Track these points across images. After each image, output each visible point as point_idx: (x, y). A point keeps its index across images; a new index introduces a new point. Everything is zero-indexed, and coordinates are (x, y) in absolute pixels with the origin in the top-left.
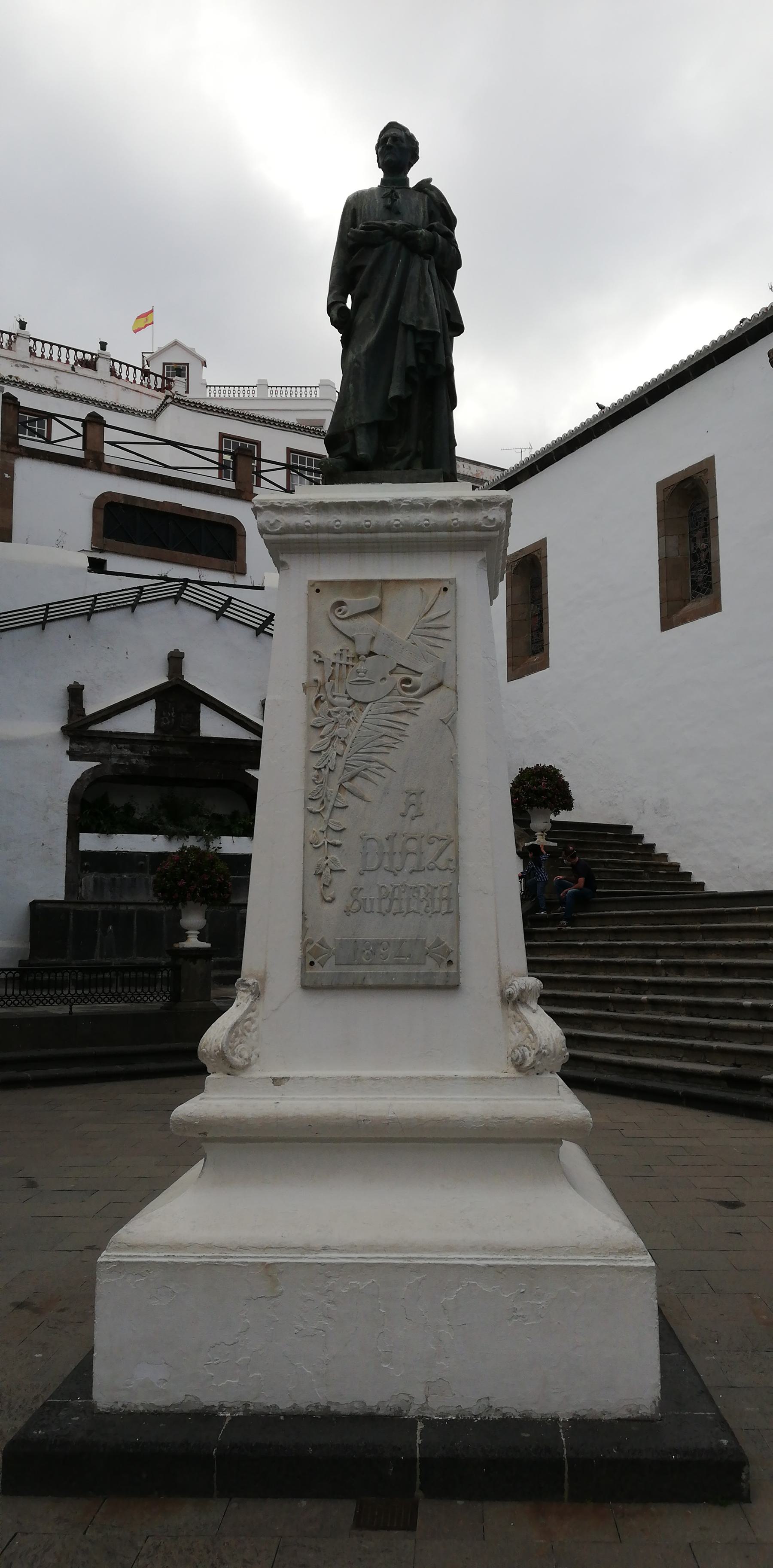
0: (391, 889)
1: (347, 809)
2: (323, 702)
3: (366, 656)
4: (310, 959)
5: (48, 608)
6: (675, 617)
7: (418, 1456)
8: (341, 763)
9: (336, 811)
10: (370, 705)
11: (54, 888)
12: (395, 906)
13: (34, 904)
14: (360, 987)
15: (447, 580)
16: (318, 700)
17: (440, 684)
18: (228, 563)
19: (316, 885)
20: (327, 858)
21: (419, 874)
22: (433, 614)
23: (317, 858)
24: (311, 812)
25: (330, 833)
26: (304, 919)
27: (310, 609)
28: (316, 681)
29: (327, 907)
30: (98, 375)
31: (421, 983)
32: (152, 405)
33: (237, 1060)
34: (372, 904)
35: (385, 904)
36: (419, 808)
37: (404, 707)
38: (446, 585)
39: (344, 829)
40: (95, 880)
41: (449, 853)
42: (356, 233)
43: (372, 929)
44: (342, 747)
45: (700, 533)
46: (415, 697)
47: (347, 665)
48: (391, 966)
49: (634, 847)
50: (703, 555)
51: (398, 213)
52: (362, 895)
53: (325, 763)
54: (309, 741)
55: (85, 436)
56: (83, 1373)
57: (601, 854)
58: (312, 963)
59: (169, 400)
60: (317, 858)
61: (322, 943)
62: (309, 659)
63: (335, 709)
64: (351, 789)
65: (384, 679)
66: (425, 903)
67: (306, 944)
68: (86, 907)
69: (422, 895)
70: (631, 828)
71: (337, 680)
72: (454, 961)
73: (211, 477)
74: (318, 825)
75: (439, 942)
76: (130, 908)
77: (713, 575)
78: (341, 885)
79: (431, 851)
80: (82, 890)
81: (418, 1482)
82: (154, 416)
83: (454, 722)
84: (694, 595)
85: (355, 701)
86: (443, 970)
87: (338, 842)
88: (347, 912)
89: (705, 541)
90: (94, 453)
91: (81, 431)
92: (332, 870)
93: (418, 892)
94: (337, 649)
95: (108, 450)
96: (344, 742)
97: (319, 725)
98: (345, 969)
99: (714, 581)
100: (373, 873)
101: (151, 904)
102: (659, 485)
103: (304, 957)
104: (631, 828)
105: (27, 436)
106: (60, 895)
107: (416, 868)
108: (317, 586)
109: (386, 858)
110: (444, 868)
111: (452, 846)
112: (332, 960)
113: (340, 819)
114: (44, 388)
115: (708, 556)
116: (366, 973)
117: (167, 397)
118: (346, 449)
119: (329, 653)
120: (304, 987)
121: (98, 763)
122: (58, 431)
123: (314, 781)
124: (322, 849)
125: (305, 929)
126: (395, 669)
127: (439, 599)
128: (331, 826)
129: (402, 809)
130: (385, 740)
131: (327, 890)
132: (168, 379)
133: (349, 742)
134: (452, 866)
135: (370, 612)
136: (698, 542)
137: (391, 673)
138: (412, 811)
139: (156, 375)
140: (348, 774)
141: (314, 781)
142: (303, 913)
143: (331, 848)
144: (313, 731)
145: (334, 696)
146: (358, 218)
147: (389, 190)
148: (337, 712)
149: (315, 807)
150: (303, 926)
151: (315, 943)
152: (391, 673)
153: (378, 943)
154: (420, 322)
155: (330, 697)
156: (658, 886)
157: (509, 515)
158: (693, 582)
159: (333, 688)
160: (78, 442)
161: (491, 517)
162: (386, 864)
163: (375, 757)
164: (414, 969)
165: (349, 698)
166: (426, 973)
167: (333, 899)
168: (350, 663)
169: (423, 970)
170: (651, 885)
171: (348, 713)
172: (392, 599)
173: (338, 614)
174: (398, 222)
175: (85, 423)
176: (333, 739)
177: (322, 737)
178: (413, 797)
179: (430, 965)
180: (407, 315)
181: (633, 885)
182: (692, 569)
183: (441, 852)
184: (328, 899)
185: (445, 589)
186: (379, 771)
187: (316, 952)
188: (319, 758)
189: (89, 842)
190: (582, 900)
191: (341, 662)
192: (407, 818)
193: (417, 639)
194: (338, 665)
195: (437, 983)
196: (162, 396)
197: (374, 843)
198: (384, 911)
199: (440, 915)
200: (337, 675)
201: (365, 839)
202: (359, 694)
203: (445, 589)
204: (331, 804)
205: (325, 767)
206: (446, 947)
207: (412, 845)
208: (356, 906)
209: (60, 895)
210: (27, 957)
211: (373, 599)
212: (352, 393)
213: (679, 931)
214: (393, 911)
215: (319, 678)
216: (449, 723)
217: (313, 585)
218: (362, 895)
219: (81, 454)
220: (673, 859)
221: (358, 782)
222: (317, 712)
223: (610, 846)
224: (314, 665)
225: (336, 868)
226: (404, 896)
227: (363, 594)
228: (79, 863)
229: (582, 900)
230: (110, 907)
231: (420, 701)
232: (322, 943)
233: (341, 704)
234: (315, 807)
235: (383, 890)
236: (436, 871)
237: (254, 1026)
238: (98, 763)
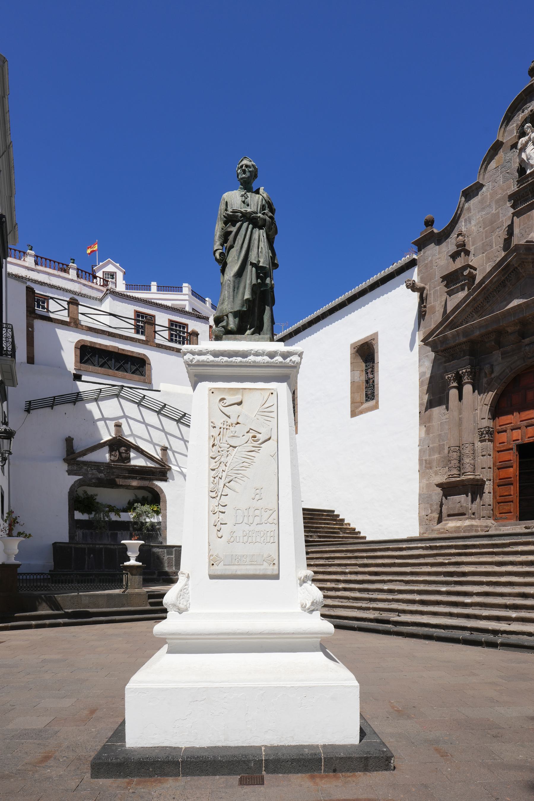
5: (55, 399)
6: (357, 411)
7: (264, 753)
8: (224, 474)
11: (64, 537)
13: (55, 544)
16: (213, 445)
18: (142, 377)
22: (266, 405)
30: (70, 277)
32: (100, 295)
33: (181, 606)
35: (246, 538)
37: (254, 449)
38: (272, 391)
40: (83, 533)
42: (228, 214)
45: (370, 370)
49: (335, 520)
50: (371, 381)
51: (248, 205)
52: (235, 535)
54: (210, 464)
55: (68, 310)
56: (119, 733)
57: (321, 523)
58: (213, 565)
59: (108, 292)
62: (209, 426)
63: (222, 449)
65: (244, 435)
66: (263, 538)
67: (210, 556)
68: (80, 546)
69: (262, 535)
70: (333, 511)
73: (131, 333)
76: (101, 546)
77: (375, 391)
79: (266, 515)
80: (77, 538)
81: (264, 769)
82: (101, 300)
84: (367, 400)
85: (231, 446)
87: (223, 511)
88: (229, 542)
89: (372, 374)
90: (74, 318)
91: (67, 307)
94: (222, 421)
95: (81, 317)
97: (214, 457)
99: (375, 394)
101: (111, 545)
102: (352, 345)
104: (333, 511)
105: (41, 309)
106: (67, 540)
109: (246, 518)
114: (44, 283)
115: (373, 382)
117: (107, 290)
118: (224, 323)
119: (218, 424)
121: (81, 477)
122: (53, 306)
125: (210, 550)
129: (253, 497)
132: (106, 280)
136: (369, 374)
137: (247, 432)
138: (257, 497)
139: (100, 278)
140: (228, 480)
146: (229, 206)
147: (244, 193)
148: (222, 451)
149: (213, 495)
152: (247, 432)
154: (259, 261)
156: (346, 538)
157: (301, 358)
158: (366, 394)
160: (66, 313)
161: (293, 360)
162: (246, 520)
163: (240, 472)
164: (258, 567)
165: (228, 444)
168: (228, 427)
169: (262, 567)
170: (343, 537)
171: (228, 451)
173: (223, 404)
174: (249, 210)
175: (69, 303)
180: (253, 258)
181: (335, 537)
182: (366, 388)
184: (220, 536)
185: (272, 393)
186: (242, 478)
189: (78, 515)
193: (259, 417)
194: (222, 428)
196: (104, 289)
202: (233, 442)
203: (272, 393)
206: (272, 557)
208: (232, 539)
209: (67, 540)
210: (53, 569)
211: (237, 398)
212: (226, 296)
213: (356, 558)
219: (68, 319)
220: (352, 526)
223: (325, 519)
226: (254, 535)
227: (234, 395)
228: (74, 524)
230: (91, 546)
231: (261, 446)
237: (187, 592)
238: (81, 477)
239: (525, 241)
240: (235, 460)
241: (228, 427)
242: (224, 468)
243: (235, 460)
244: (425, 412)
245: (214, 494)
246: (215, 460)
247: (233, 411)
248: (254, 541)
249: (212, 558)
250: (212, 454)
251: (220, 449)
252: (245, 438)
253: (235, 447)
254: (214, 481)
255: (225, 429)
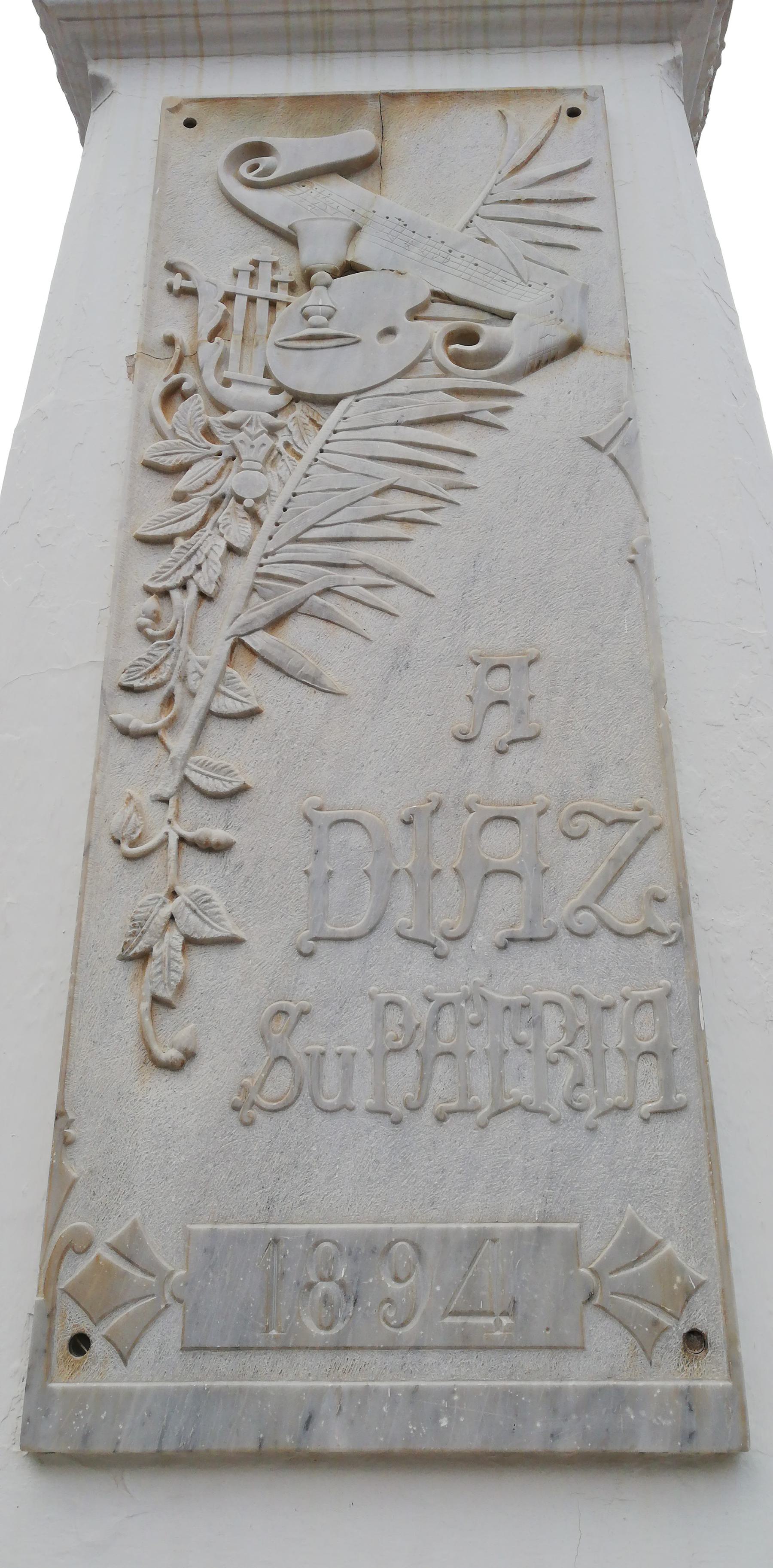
0: (423, 1013)
1: (255, 727)
2: (185, 397)
3: (335, 274)
4: (74, 1320)
8: (241, 574)
9: (214, 727)
10: (343, 404)
12: (443, 1083)
14: (291, 1456)
15: (577, 91)
16: (173, 393)
17: (574, 345)
19: (128, 996)
20: (174, 894)
21: (538, 954)
22: (539, 169)
23: (137, 894)
24: (125, 732)
25: (192, 805)
26: (64, 1142)
27: (162, 162)
28: (170, 342)
29: (162, 1086)
31: (568, 1444)
34: (347, 1080)
35: (405, 1068)
36: (522, 714)
37: (459, 405)
38: (575, 101)
39: (243, 790)
41: (649, 870)
43: (349, 1183)
44: (248, 526)
46: (495, 378)
47: (273, 304)
48: (431, 1358)
52: (304, 1041)
53: (185, 572)
58: (79, 1344)
60: (137, 894)
61: (129, 1249)
62: (150, 285)
64: (275, 655)
65: (390, 332)
66: (566, 1072)
67: (62, 1248)
71: (236, 338)
72: (715, 1335)
74: (146, 774)
75: (638, 1245)
78: (223, 1002)
79: (578, 866)
83: (632, 443)
85: (297, 398)
86: (667, 1376)
87: (217, 834)
88: (244, 1108)
92: (189, 942)
93: (537, 1023)
94: (243, 261)
96: (254, 515)
97: (170, 461)
98: (219, 1374)
100: (355, 950)
103: (48, 1314)
107: (520, 930)
108: (188, 112)
110: (632, 927)
111: (657, 846)
112: (168, 1331)
113: (231, 755)
116: (319, 1394)
119: (213, 276)
120: (43, 1460)
123: (141, 629)
124: (155, 861)
126: (424, 306)
127: (554, 136)
128: (195, 778)
130: (397, 502)
131: (168, 1019)
133: (269, 513)
134: (665, 920)
135: (349, 169)
137: (415, 314)
140: (267, 609)
141: (141, 629)
142: (60, 1115)
143: (191, 856)
144: (152, 479)
145: (227, 383)
148: (235, 427)
149: (141, 713)
150: (56, 1172)
151: (100, 1250)
152: (415, 314)
153: (375, 1250)
155: (212, 382)
159: (223, 361)
162: (402, 915)
163: (359, 552)
164: (533, 1375)
165: (277, 390)
166: (594, 1394)
167: (189, 1055)
168: (281, 294)
169: (578, 1376)
171: (272, 431)
172: (411, 144)
176: (216, 503)
177: (181, 497)
178: (500, 678)
179: (603, 1356)
183: (620, 867)
184: (169, 1054)
185: (574, 113)
187: (102, 1293)
188: (166, 557)
190: (389, 1300)
191: (254, 292)
192: (481, 750)
193: (496, 231)
194: (241, 302)
195: (645, 1445)
197: (355, 837)
198: (396, 1108)
199: (633, 1120)
200: (238, 324)
201: (323, 822)
202: (309, 373)
203: (574, 113)
204: (200, 702)
205: (184, 587)
206: (670, 1267)
207: (501, 844)
208: (281, 1081)
211: (356, 141)
214: (433, 1105)
215: (183, 336)
216: (613, 446)
217: (176, 109)
218: (304, 1041)
221: (300, 633)
222: (166, 426)
224: (168, 301)
225: (208, 932)
226: (479, 1040)
229: (389, 1300)
231: (512, 387)
232: (129, 1249)
233: (248, 405)
234: (141, 713)
235: (394, 1016)
236: (604, 941)
239: (160, 566)
240: (323, 476)
241: (281, 294)
242: (238, 530)
243: (323, 476)
244: (583, 438)
245: (147, 702)
246: (183, 483)
247: (322, 213)
248: (482, 1095)
249: (75, 1269)
250: (151, 449)
251: (216, 420)
252: (391, 356)
253: (332, 401)
254: (156, 618)
255: (262, 307)
